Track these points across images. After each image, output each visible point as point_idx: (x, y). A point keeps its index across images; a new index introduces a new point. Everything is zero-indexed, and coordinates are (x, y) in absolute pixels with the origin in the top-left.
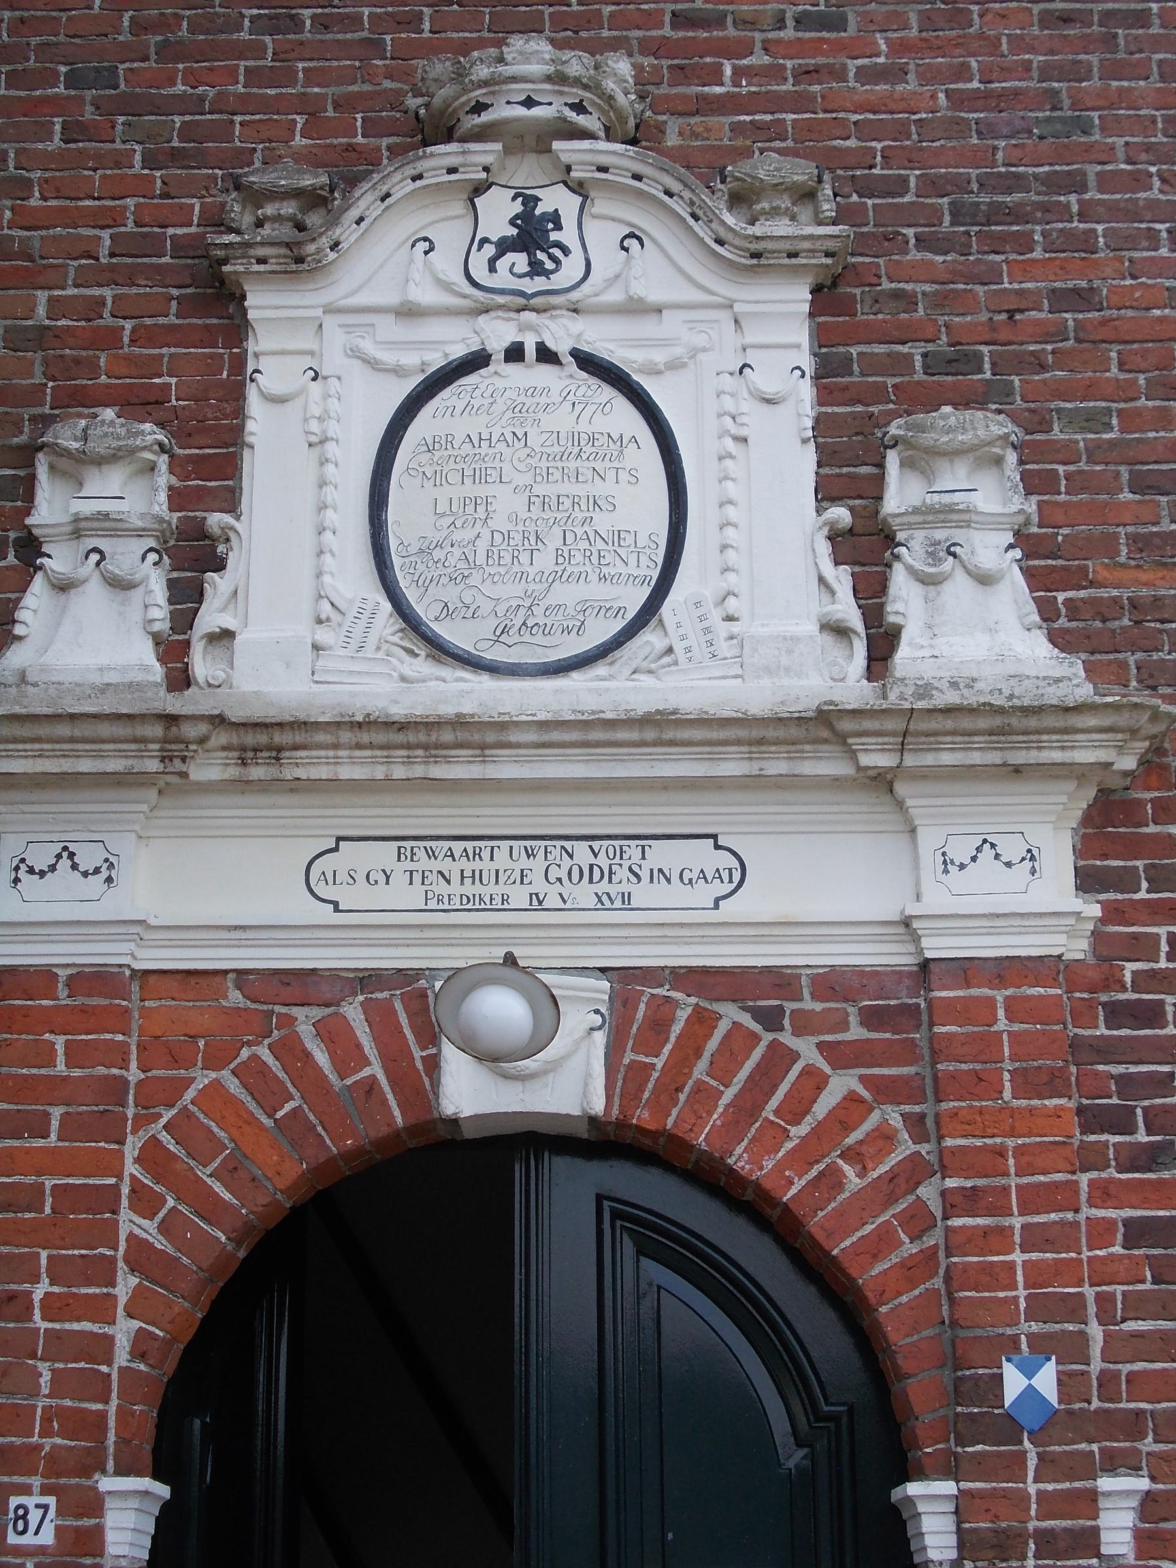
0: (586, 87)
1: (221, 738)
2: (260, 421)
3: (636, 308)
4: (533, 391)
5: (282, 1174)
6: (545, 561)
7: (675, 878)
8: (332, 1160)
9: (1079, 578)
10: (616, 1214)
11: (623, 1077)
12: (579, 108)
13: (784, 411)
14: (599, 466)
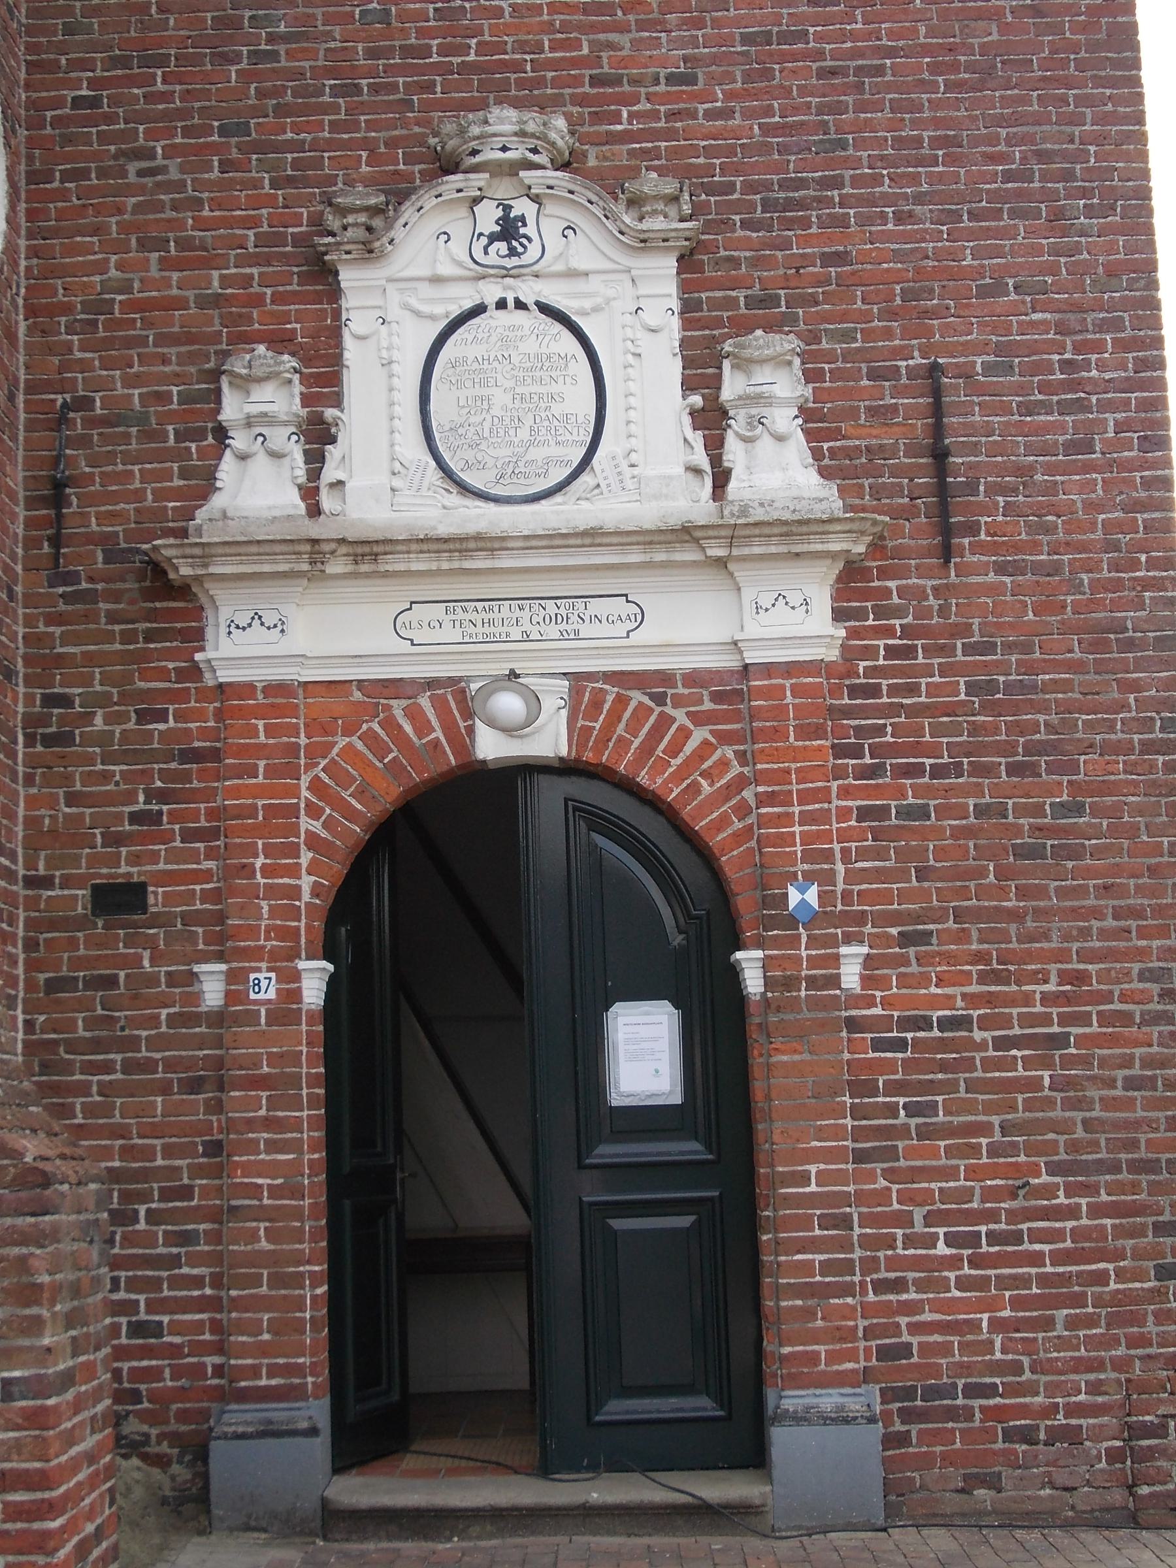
0: (538, 138)
1: (343, 549)
2: (352, 351)
3: (572, 274)
4: (512, 328)
5: (389, 794)
6: (523, 434)
7: (604, 620)
8: (417, 785)
9: (835, 435)
10: (576, 809)
11: (578, 735)
12: (535, 151)
13: (662, 337)
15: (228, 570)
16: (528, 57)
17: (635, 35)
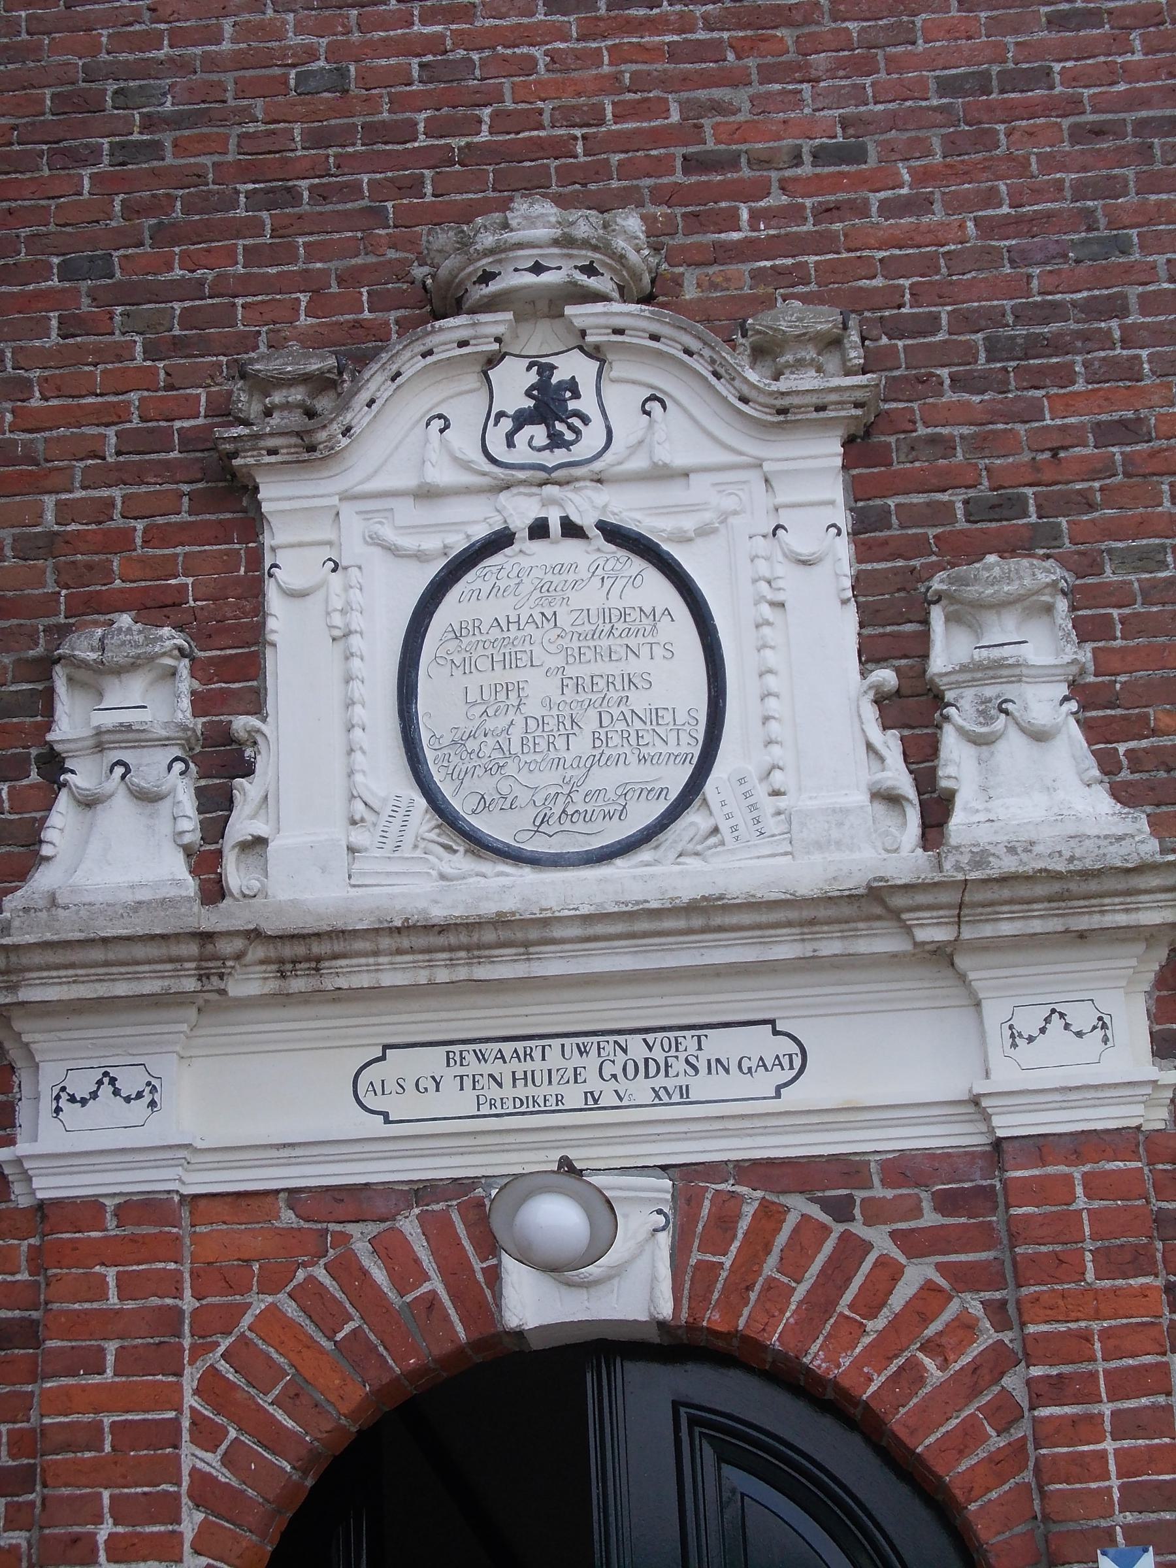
0: (595, 248)
1: (258, 952)
2: (281, 618)
3: (661, 474)
5: (345, 1398)
6: (582, 745)
7: (733, 1068)
9: (1138, 728)
10: (697, 1422)
11: (690, 1278)
12: (590, 270)
15: (51, 994)
16: (578, 132)
17: (757, 89)
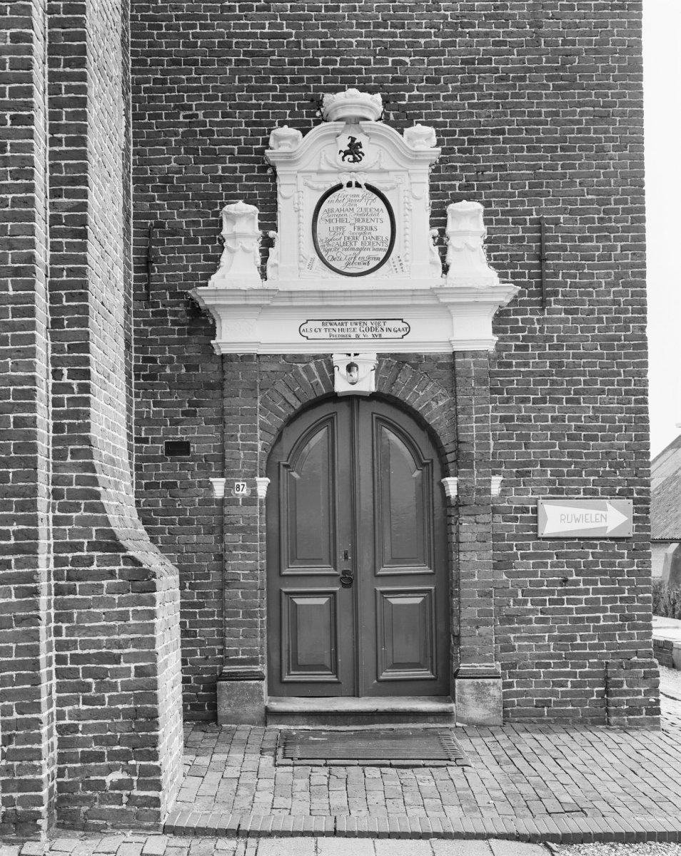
3: (382, 171)
9: (497, 249)
14: (373, 218)
